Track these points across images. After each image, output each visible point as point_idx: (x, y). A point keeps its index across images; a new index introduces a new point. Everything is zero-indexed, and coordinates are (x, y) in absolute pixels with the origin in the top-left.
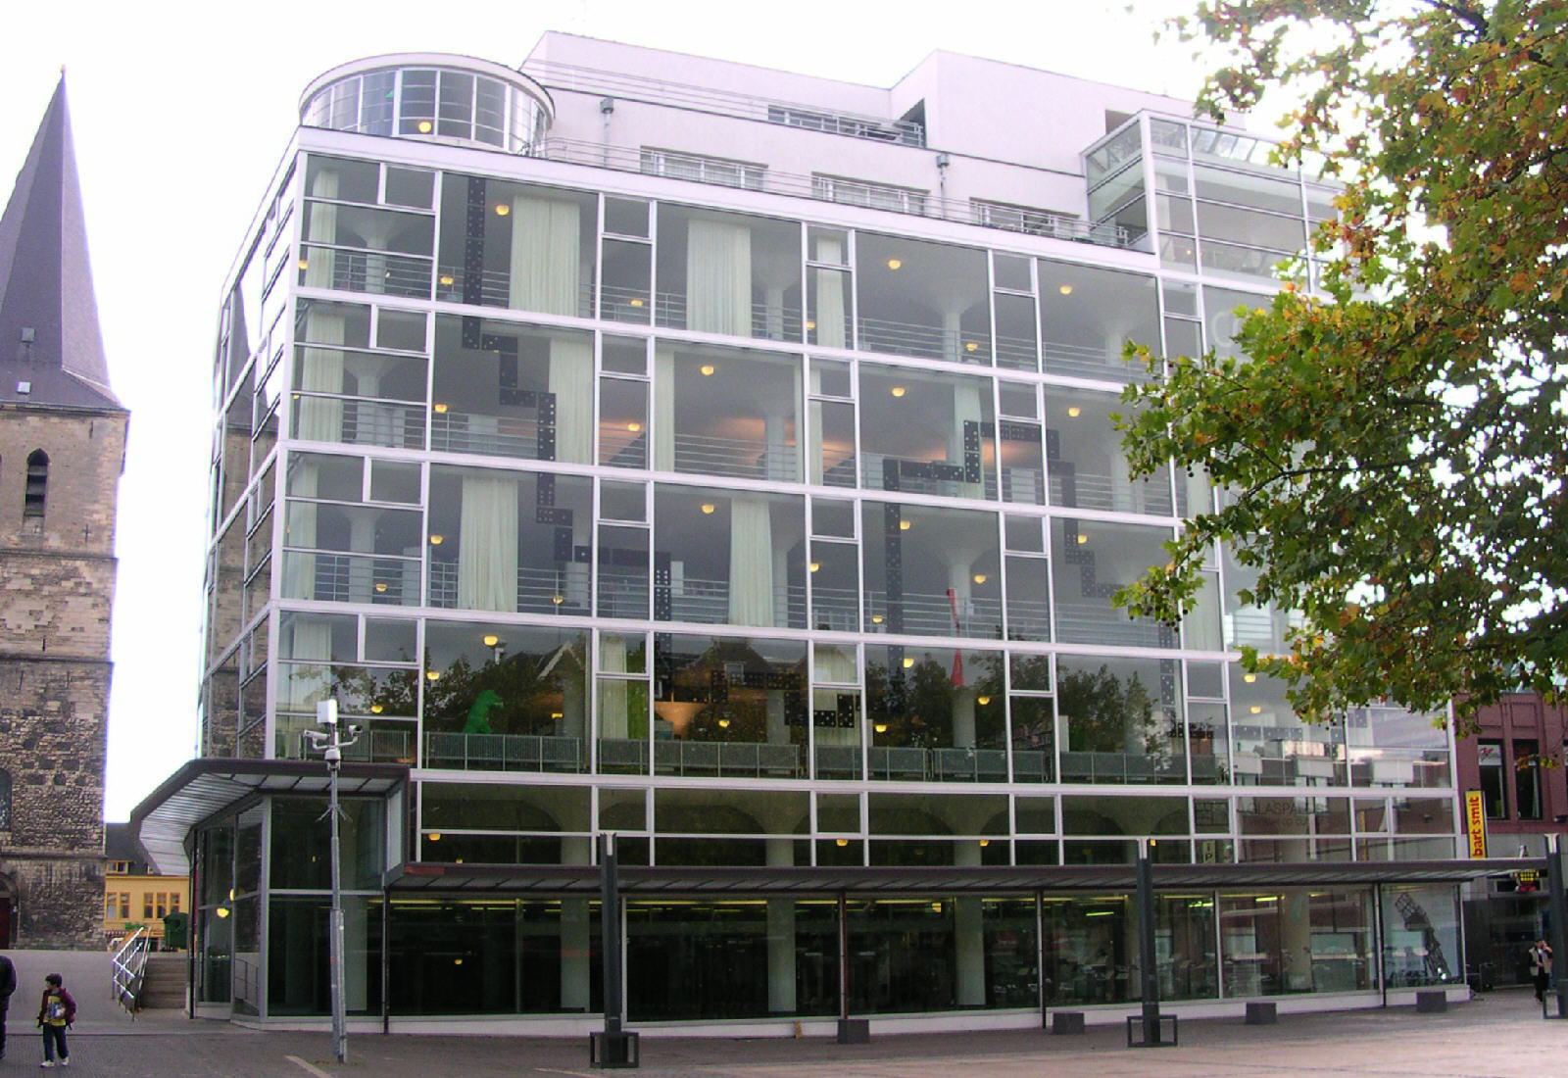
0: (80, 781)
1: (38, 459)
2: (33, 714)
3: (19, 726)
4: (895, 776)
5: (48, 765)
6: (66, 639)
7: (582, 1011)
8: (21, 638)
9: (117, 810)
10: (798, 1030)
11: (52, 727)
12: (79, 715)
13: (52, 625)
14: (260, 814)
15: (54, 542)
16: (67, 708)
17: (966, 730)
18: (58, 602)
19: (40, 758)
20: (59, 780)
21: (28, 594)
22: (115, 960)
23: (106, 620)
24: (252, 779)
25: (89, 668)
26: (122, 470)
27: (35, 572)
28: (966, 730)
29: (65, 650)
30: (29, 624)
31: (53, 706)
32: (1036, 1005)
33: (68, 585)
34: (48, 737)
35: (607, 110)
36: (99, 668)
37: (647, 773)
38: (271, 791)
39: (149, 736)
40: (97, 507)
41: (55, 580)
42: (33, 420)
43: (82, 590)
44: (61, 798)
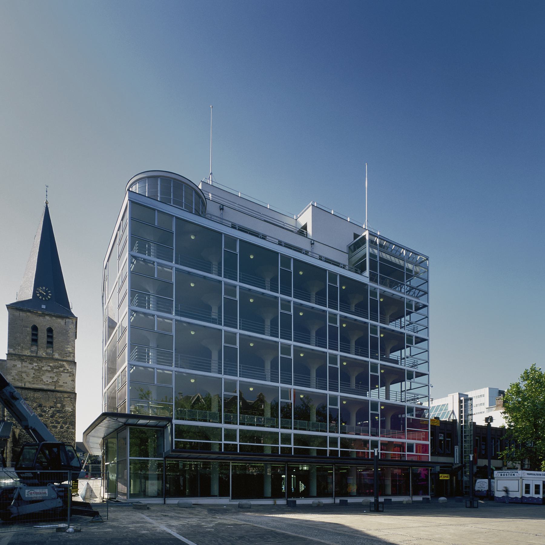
0: (68, 428)
1: (50, 330)
2: (53, 407)
3: (49, 411)
4: (300, 429)
5: (59, 423)
6: (61, 386)
7: (216, 496)
8: (48, 385)
9: (79, 438)
10: (275, 502)
11: (59, 411)
12: (67, 409)
13: (57, 382)
14: (129, 430)
15: (57, 356)
16: (63, 406)
17: (314, 418)
18: (58, 374)
19: (56, 421)
20: (62, 427)
21: (49, 371)
22: (199, 394)
23: (74, 381)
24: (123, 420)
25: (69, 394)
26: (76, 338)
27: (51, 365)
28: (314, 418)
29: (61, 389)
30: (50, 381)
31: (59, 405)
32: (409, 495)
33: (62, 369)
34: (58, 414)
35: (222, 209)
36: (73, 395)
37: (237, 424)
38: (130, 425)
39: (89, 405)
40: (69, 346)
41: (58, 367)
42: (47, 318)
43: (66, 371)
44: (63, 433)
